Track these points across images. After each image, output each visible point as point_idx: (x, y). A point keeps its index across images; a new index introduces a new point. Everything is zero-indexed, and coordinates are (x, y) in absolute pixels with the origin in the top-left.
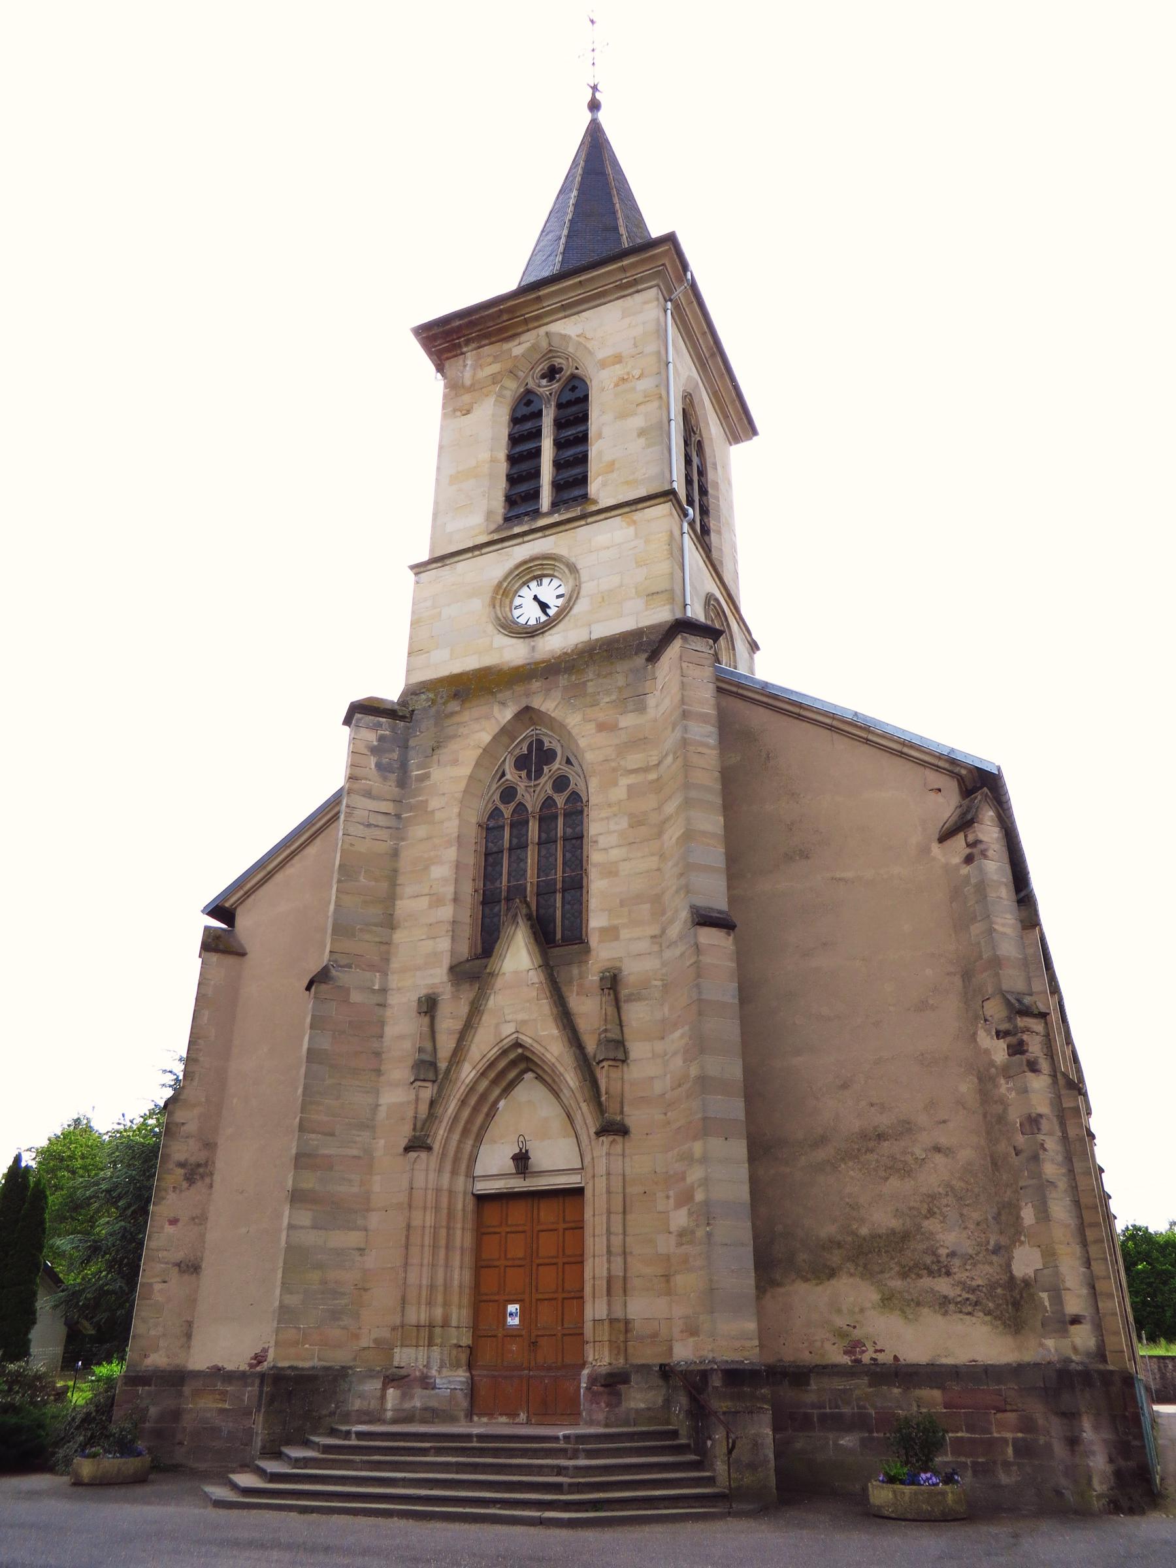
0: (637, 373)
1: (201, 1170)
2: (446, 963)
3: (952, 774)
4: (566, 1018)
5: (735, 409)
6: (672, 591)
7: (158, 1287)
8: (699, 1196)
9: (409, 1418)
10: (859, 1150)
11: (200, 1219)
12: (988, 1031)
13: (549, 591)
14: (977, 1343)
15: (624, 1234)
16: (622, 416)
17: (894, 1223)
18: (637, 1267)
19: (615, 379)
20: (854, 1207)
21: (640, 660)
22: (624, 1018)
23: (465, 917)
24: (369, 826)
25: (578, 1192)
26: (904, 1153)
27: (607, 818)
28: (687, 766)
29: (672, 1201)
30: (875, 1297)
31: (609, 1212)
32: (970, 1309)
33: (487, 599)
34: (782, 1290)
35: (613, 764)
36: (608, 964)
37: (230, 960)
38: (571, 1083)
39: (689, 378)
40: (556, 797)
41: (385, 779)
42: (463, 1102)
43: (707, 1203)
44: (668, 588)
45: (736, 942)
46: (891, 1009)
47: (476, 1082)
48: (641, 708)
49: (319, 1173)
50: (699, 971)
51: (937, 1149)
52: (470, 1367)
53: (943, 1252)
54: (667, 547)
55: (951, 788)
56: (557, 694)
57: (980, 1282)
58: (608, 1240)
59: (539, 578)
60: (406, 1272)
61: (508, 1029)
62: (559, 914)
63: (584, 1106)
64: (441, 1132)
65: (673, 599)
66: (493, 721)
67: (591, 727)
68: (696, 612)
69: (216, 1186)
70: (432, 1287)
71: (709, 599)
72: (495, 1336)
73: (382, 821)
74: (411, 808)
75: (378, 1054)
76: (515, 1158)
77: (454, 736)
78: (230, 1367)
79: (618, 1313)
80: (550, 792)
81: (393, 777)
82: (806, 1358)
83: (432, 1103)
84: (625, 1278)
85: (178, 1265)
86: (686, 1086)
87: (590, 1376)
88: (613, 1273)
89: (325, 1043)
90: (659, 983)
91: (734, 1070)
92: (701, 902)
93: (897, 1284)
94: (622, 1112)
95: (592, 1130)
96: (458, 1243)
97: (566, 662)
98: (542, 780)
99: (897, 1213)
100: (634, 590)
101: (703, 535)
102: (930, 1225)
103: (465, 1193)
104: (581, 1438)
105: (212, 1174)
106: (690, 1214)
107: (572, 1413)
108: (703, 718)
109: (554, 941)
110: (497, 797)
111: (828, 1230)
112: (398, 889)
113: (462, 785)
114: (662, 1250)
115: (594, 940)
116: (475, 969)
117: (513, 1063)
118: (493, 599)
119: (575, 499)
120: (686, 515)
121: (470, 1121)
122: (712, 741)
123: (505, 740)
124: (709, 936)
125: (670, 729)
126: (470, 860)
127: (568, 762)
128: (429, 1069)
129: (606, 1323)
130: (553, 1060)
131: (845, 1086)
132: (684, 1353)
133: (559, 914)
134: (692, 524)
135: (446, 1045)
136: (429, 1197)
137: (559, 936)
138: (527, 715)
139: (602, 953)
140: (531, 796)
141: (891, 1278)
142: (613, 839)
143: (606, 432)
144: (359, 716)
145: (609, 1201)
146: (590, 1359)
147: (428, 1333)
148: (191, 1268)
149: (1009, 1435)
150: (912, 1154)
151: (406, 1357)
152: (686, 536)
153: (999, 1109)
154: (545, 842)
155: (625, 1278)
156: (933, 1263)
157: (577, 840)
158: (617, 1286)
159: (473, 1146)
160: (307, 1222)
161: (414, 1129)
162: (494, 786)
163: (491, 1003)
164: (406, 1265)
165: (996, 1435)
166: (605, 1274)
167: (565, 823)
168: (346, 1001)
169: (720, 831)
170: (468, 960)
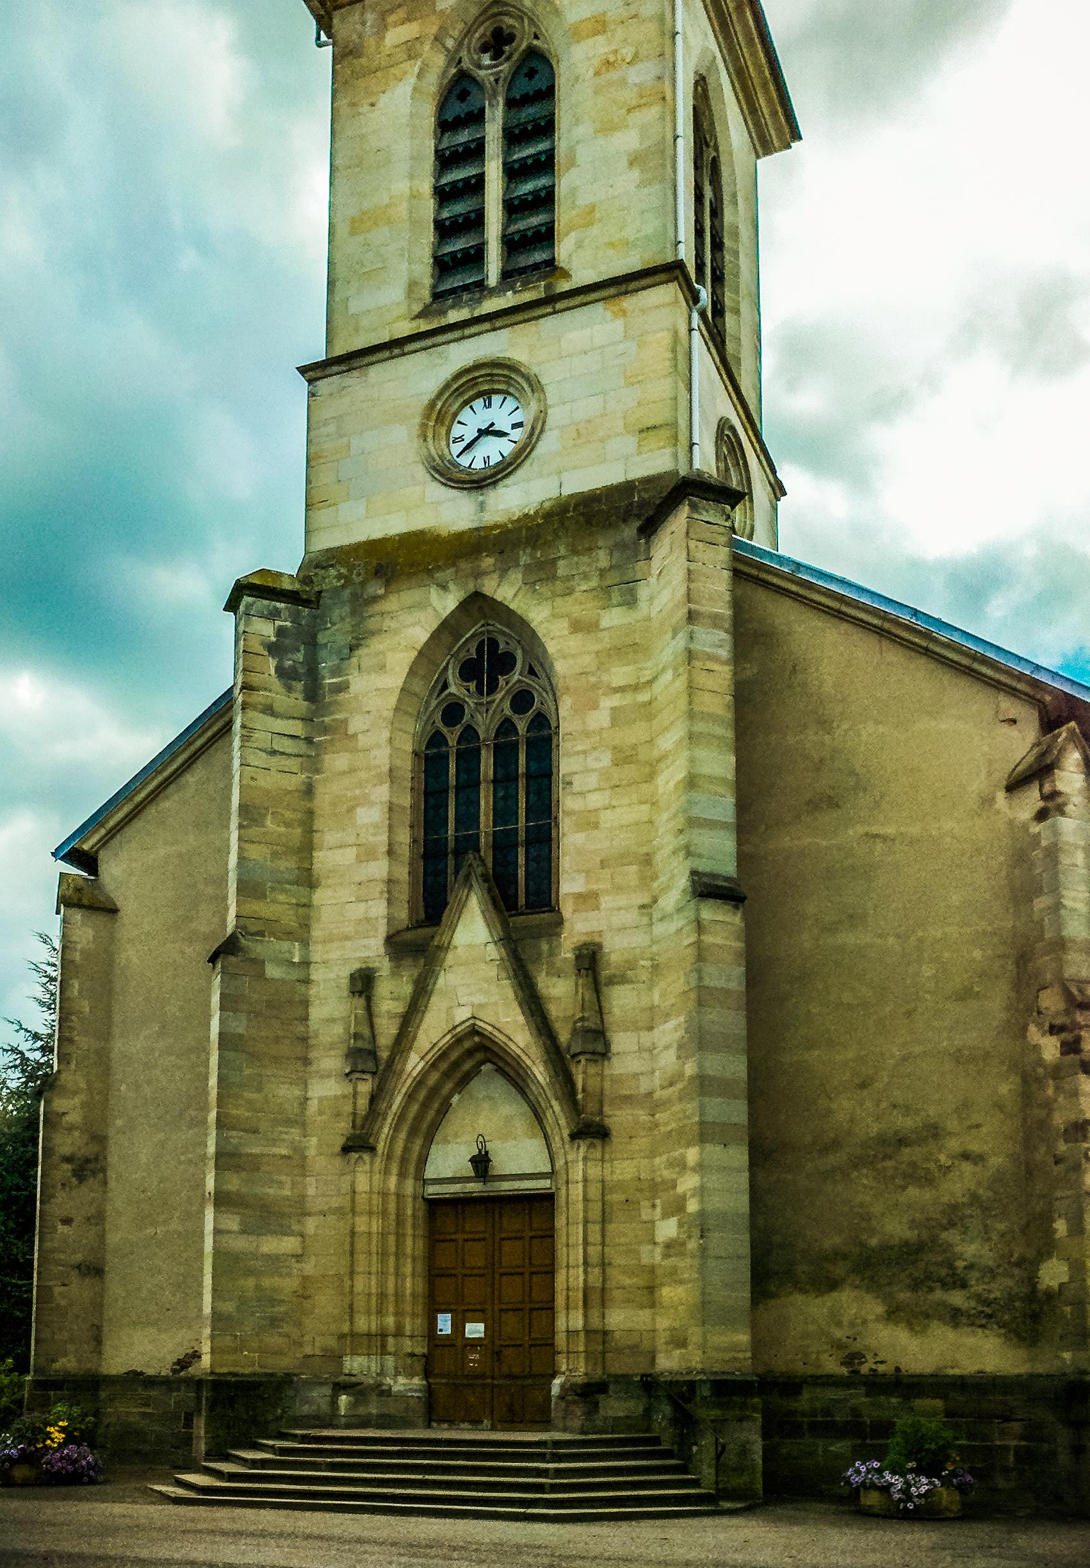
0: (628, 52)
1: (91, 1166)
2: (382, 931)
3: (1033, 701)
4: (533, 1004)
5: (769, 101)
6: (674, 425)
7: (58, 1290)
8: (692, 1206)
9: (365, 1424)
10: (875, 1156)
11: (98, 1218)
12: (1039, 1025)
13: (501, 413)
14: (985, 1353)
15: (603, 1244)
16: (607, 128)
17: (910, 1235)
18: (618, 1278)
19: (596, 62)
20: (867, 1217)
21: (629, 531)
22: (603, 1004)
23: (403, 873)
24: (274, 753)
25: (548, 1198)
26: (927, 1160)
27: (584, 752)
28: (692, 689)
29: (658, 1210)
30: (880, 1309)
31: (586, 1222)
32: (984, 1321)
33: (416, 430)
34: (772, 1302)
35: (593, 679)
36: (584, 939)
37: (100, 919)
38: (540, 1078)
39: (705, 50)
40: (515, 718)
41: (290, 689)
42: (410, 1097)
43: (702, 1214)
44: (670, 420)
45: (745, 918)
46: (928, 996)
47: (425, 1074)
48: (630, 601)
49: (244, 1174)
50: (701, 953)
51: (965, 1156)
52: (427, 1374)
53: (960, 1264)
54: (669, 355)
55: (1029, 720)
56: (516, 576)
57: (998, 1294)
58: (585, 1250)
59: (487, 395)
60: (352, 1279)
61: (462, 1014)
62: (521, 873)
63: (555, 1103)
64: (386, 1130)
65: (676, 439)
66: (430, 610)
67: (561, 627)
68: (705, 460)
69: (112, 1184)
70: (382, 1296)
71: (724, 430)
72: (453, 1345)
73: (287, 746)
74: (325, 729)
75: (304, 1040)
76: (473, 1160)
77: (379, 631)
78: (150, 1372)
79: (595, 1323)
80: (508, 712)
81: (299, 686)
82: (799, 1368)
83: (374, 1099)
84: (603, 1289)
85: (79, 1267)
86: (680, 1086)
87: (562, 1386)
88: (590, 1284)
89: (239, 1026)
90: (648, 963)
91: (737, 1067)
92: (704, 866)
93: (904, 1296)
94: (601, 1112)
95: (566, 1133)
96: (409, 1251)
97: (529, 529)
98: (499, 696)
99: (913, 1224)
100: (621, 423)
101: (717, 338)
102: (951, 1236)
103: (415, 1198)
104: (557, 1444)
105: (103, 1170)
106: (680, 1225)
107: (545, 1423)
108: (715, 621)
109: (515, 907)
110: (438, 716)
111: (833, 1241)
112: (316, 836)
113: (393, 700)
114: (645, 1260)
115: (567, 909)
116: (418, 940)
117: (470, 1053)
118: (424, 426)
119: (536, 267)
120: (696, 298)
121: (419, 1118)
122: (724, 653)
123: (446, 638)
124: (711, 912)
125: (670, 634)
126: (406, 800)
127: (532, 672)
128: (368, 1059)
129: (582, 1335)
130: (519, 1052)
131: (863, 1086)
132: (668, 1362)
133: (521, 873)
134: (703, 314)
135: (387, 1030)
136: (375, 1202)
137: (522, 900)
138: (477, 604)
139: (578, 925)
140: (486, 715)
141: (901, 1290)
142: (592, 780)
143: (583, 155)
144: (250, 599)
145: (585, 1211)
146: (564, 1368)
147: (377, 1342)
148: (94, 1270)
149: (1013, 1443)
150: (937, 1161)
151: (356, 1364)
152: (696, 335)
153: (1041, 1113)
154: (505, 779)
155: (603, 1289)
156: (948, 1275)
157: (543, 779)
158: (595, 1298)
159: (423, 1146)
160: (235, 1227)
161: (354, 1127)
162: (434, 703)
163: (441, 981)
164: (352, 1273)
165: (998, 1443)
166: (581, 1285)
167: (530, 756)
168: (261, 975)
169: (730, 775)
170: (408, 929)
